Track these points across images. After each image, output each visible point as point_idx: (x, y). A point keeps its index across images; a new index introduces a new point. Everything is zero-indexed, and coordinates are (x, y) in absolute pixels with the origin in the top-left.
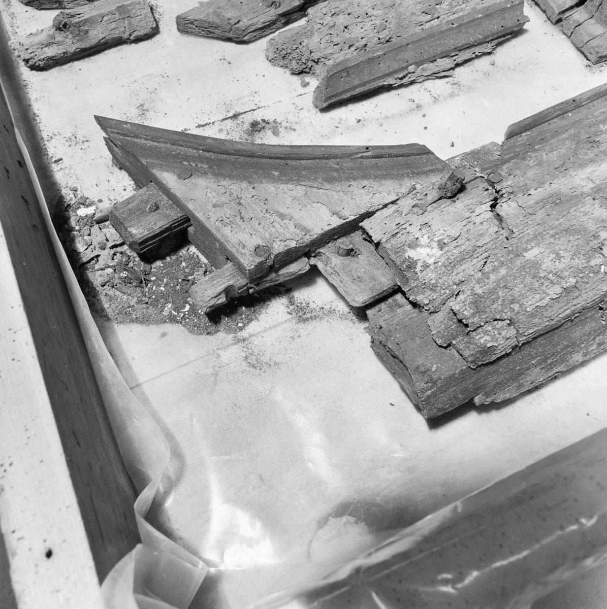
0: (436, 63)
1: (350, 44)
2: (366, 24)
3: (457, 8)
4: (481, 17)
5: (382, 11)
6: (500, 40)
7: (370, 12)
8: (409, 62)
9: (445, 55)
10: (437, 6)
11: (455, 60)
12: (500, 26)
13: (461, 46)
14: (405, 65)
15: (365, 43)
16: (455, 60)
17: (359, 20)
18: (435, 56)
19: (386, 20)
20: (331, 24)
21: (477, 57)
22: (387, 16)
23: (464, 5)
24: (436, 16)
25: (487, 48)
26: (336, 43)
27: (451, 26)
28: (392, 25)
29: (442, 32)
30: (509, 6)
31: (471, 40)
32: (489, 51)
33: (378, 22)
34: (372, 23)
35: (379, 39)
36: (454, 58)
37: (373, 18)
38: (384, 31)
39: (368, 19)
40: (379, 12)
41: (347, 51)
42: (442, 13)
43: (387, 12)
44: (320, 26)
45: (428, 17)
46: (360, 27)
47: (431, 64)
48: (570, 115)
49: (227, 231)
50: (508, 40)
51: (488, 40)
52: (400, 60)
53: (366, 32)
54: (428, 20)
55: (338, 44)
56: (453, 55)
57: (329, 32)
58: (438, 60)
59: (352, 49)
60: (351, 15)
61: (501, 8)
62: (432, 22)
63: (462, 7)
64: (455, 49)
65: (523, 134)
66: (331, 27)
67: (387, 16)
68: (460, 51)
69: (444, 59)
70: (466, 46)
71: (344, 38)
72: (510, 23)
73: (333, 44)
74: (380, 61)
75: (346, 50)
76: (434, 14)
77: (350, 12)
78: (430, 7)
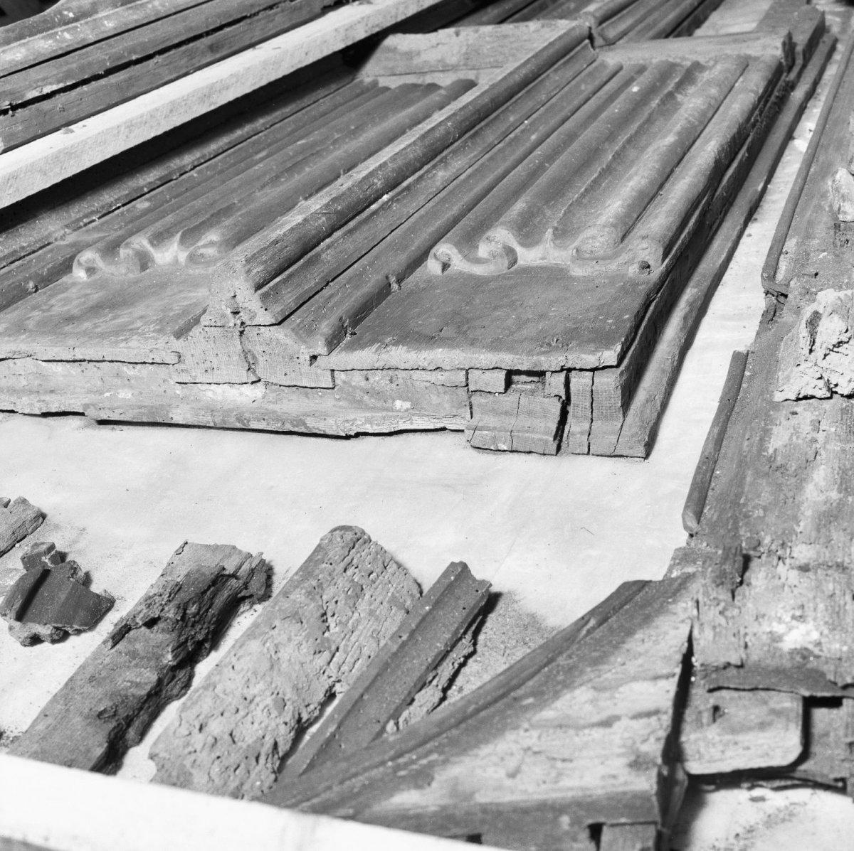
0: (416, 704)
1: (256, 755)
2: (254, 713)
3: (350, 622)
4: (430, 610)
5: (262, 683)
6: (473, 628)
7: (250, 693)
8: (382, 721)
9: (422, 685)
10: (327, 634)
11: (437, 686)
12: (461, 609)
13: (433, 661)
14: (378, 727)
15: (272, 741)
16: (437, 686)
17: (242, 713)
18: (410, 693)
19: (276, 692)
20: (211, 740)
21: (463, 665)
22: (273, 686)
23: (356, 615)
24: (334, 648)
25: (465, 646)
26: (235, 767)
27: (400, 641)
28: (289, 694)
29: (395, 654)
30: (452, 578)
31: (440, 646)
32: (471, 649)
33: (269, 701)
34: (261, 706)
35: (286, 724)
36: (435, 682)
37: (257, 700)
38: (286, 708)
39: (253, 706)
40: (261, 686)
41: (258, 768)
42: (339, 640)
43: (269, 679)
44: (193, 757)
45: (326, 655)
46: (249, 723)
47: (411, 708)
48: (718, 472)
49: (566, 782)
50: (482, 623)
51: (459, 635)
52: (365, 724)
53: (263, 725)
54: (329, 660)
55: (238, 766)
56: (430, 679)
57: (214, 756)
58: (417, 697)
59: (262, 761)
60: (225, 714)
61: (446, 586)
62: (335, 659)
63: (354, 618)
64: (428, 669)
65: (705, 511)
66: (213, 746)
67: (273, 686)
68: (435, 668)
69: (423, 692)
70: (440, 657)
71: (241, 751)
72: (471, 600)
73: (232, 769)
74: (339, 740)
75: (255, 767)
76: (329, 648)
77: (221, 710)
78: (318, 641)
